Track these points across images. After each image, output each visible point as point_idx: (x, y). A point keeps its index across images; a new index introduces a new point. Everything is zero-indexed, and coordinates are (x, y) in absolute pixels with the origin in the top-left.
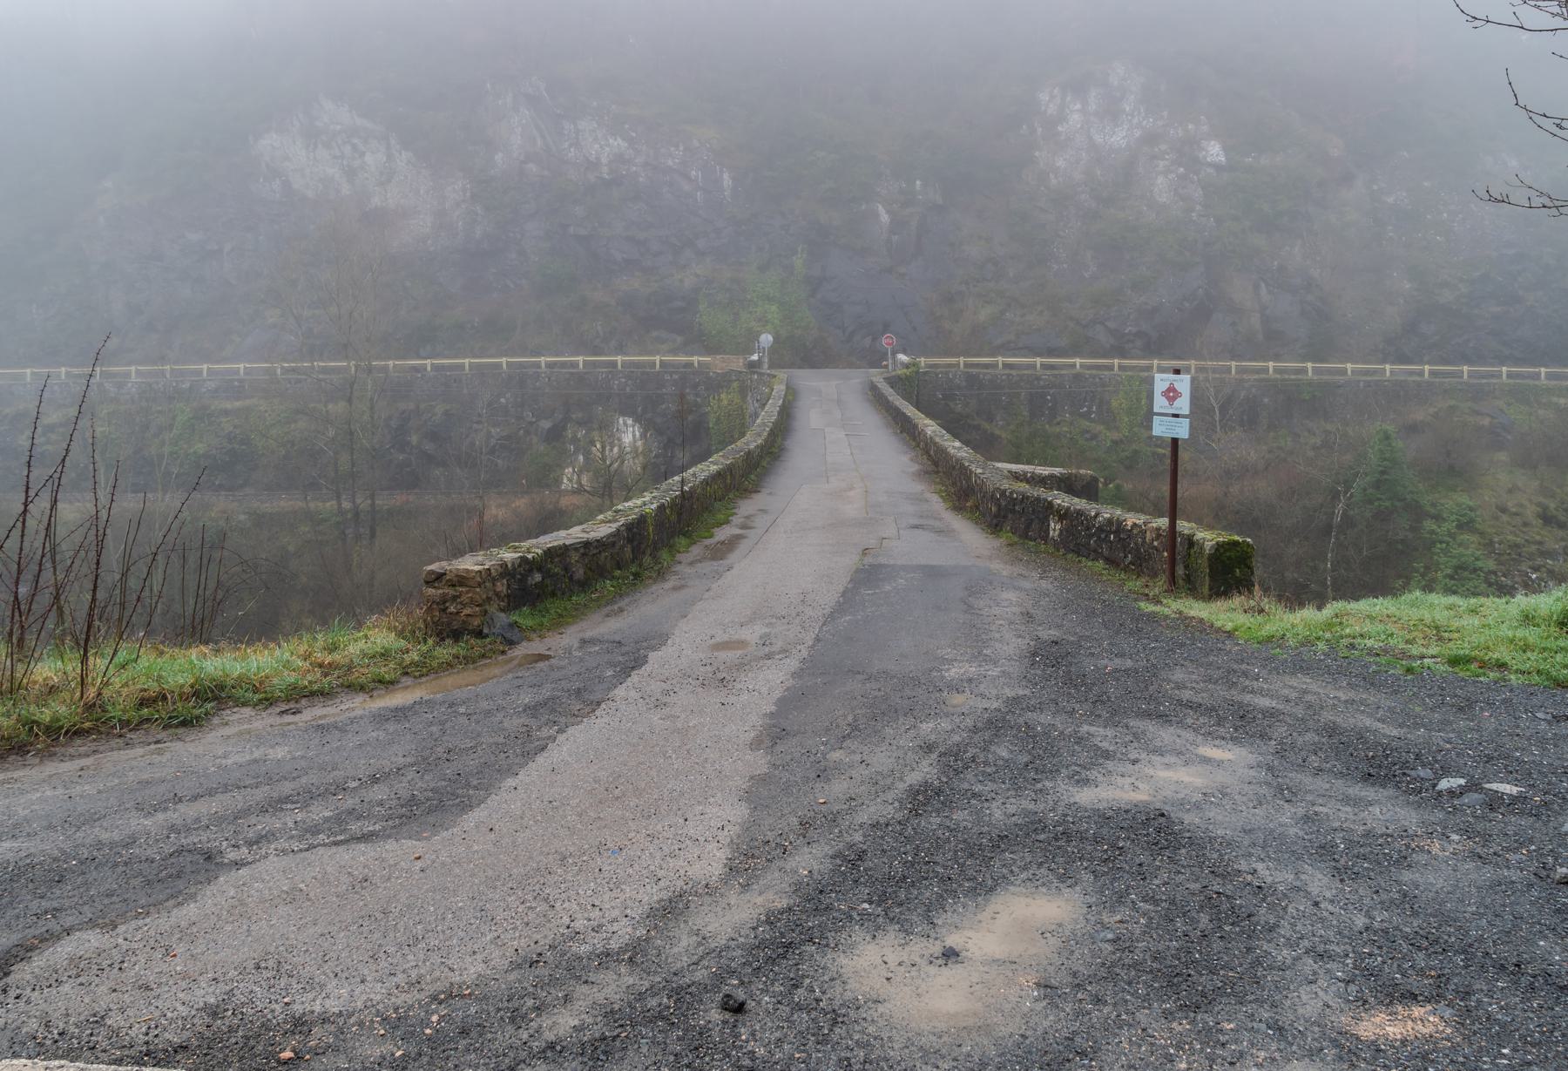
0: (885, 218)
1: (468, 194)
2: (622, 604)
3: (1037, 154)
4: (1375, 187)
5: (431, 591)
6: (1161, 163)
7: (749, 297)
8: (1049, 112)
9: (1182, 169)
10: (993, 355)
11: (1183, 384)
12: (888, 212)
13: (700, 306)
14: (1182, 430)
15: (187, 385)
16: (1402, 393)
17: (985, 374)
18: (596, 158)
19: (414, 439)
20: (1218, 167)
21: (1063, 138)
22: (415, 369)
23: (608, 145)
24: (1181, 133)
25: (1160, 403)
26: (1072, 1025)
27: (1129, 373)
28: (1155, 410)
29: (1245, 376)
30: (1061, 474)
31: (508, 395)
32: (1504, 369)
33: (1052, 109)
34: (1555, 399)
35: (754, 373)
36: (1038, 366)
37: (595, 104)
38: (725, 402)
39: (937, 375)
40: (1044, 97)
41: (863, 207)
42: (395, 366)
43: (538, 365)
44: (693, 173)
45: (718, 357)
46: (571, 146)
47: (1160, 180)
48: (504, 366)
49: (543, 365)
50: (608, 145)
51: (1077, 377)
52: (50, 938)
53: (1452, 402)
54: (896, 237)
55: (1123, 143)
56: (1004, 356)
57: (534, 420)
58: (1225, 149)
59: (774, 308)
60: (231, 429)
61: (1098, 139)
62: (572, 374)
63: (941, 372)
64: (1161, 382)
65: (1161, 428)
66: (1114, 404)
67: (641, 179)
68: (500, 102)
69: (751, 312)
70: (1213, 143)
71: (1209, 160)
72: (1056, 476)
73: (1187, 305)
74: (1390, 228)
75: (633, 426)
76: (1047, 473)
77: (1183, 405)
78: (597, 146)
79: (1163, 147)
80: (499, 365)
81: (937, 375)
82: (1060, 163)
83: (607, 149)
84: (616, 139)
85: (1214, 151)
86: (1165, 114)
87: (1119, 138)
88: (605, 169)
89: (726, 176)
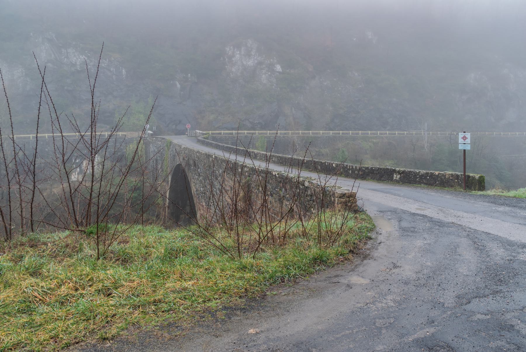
0: (179, 86)
1: (24, 74)
3: (226, 67)
4: (321, 80)
5: (342, 200)
6: (264, 71)
7: (133, 112)
8: (229, 54)
9: (270, 73)
10: (232, 130)
11: (468, 135)
12: (180, 84)
13: (116, 115)
14: (468, 148)
16: (335, 139)
17: (218, 136)
18: (75, 63)
20: (279, 72)
21: (234, 62)
23: (80, 58)
24: (269, 62)
25: (461, 141)
27: (261, 135)
29: (294, 135)
32: (360, 132)
33: (230, 53)
34: (373, 140)
35: (154, 137)
36: (234, 133)
37: (74, 43)
38: (131, 148)
40: (228, 49)
41: (172, 82)
42: (370, 133)
44: (112, 69)
45: (129, 132)
46: (65, 58)
47: (263, 76)
50: (80, 58)
51: (246, 137)
53: (348, 142)
54: (182, 92)
55: (252, 64)
56: (223, 130)
58: (282, 67)
59: (142, 116)
61: (245, 63)
62: (74, 139)
64: (461, 135)
65: (461, 147)
66: (257, 145)
67: (92, 71)
68: (37, 41)
69: (134, 117)
70: (278, 65)
73: (272, 114)
74: (326, 92)
75: (98, 157)
77: (468, 141)
78: (75, 58)
79: (264, 66)
82: (233, 70)
83: (79, 59)
84: (83, 56)
86: (264, 56)
87: (250, 63)
88: (78, 66)
89: (124, 71)
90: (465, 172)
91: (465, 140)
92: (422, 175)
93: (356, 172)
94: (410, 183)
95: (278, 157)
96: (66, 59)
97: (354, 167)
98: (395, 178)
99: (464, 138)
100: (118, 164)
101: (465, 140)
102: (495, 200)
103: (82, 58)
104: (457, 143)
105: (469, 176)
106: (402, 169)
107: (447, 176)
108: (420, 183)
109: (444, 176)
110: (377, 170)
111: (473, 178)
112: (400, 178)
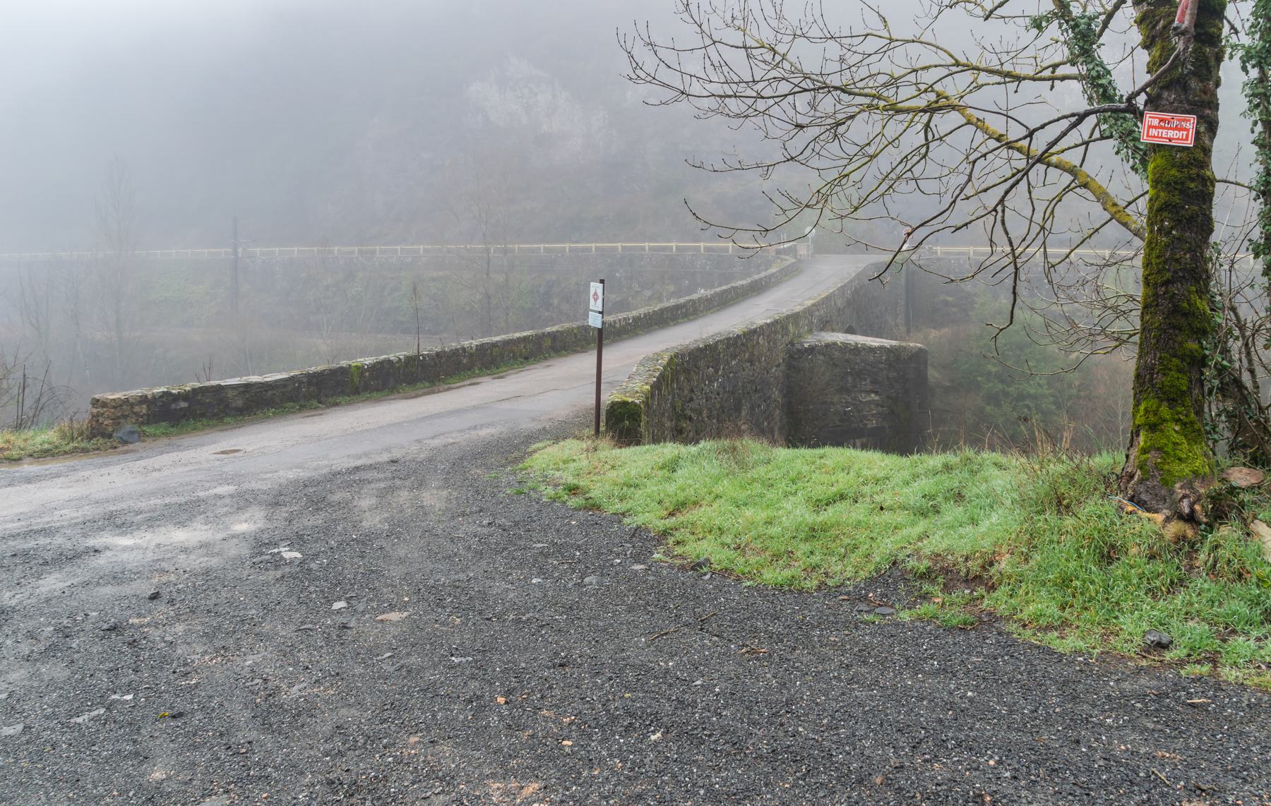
2: (339, 399)
15: (410, 260)
19: (555, 302)
22: (584, 250)
28: (591, 308)
30: (891, 346)
31: (621, 271)
39: (950, 261)
43: (643, 249)
48: (620, 250)
49: (647, 248)
52: (187, 472)
57: (640, 289)
60: (436, 291)
63: (954, 259)
72: (885, 348)
76: (877, 344)
80: (616, 248)
81: (950, 261)
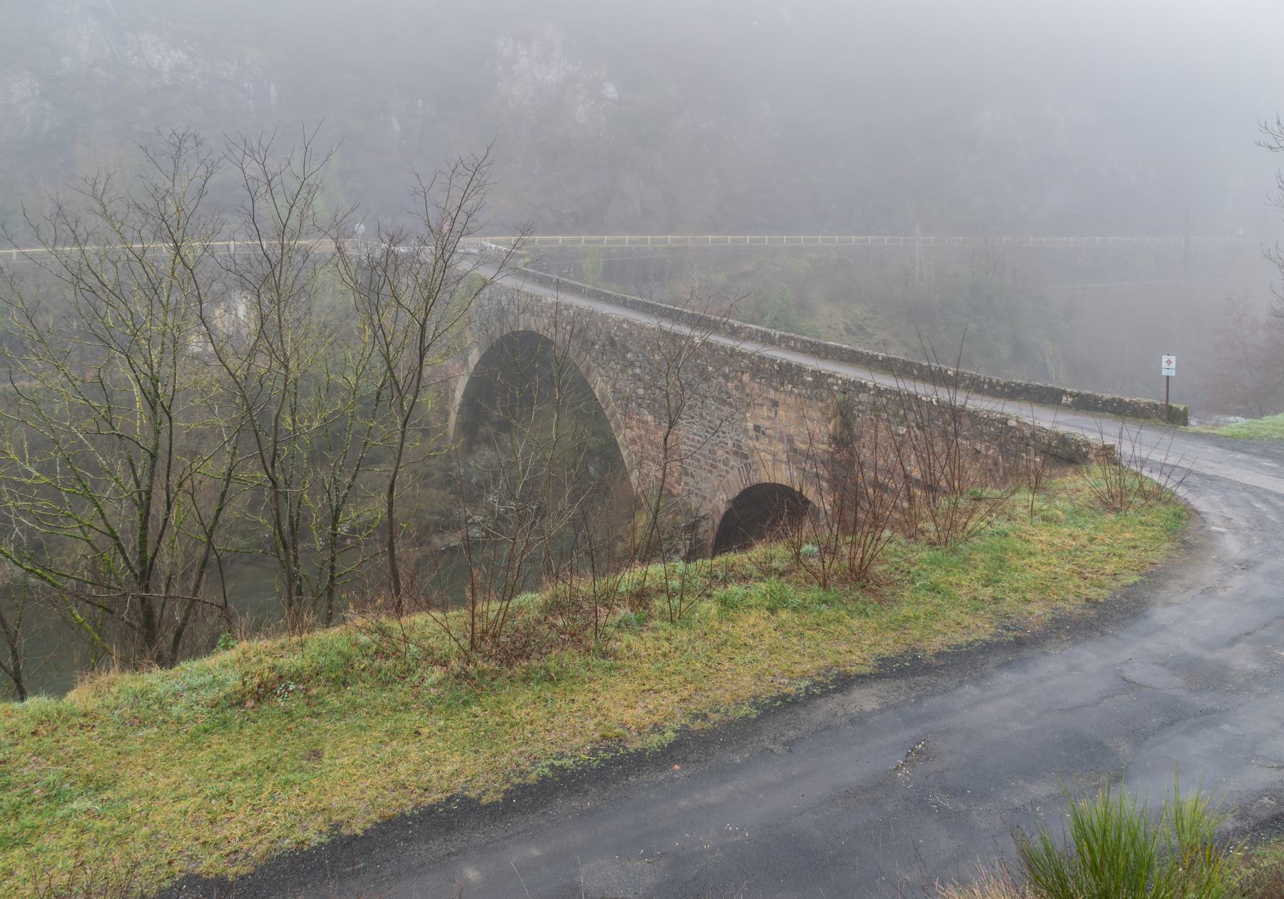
0: (397, 127)
9: (593, 102)
11: (1173, 359)
14: (1172, 373)
25: (1164, 365)
26: (73, 487)
64: (1165, 358)
65: (1165, 373)
71: (608, 95)
77: (1173, 365)
83: (169, 59)
85: (611, 90)
89: (272, 88)
90: (1167, 401)
91: (1169, 364)
92: (1107, 401)
93: (998, 388)
94: (1088, 410)
95: (803, 341)
96: (136, 58)
97: (994, 381)
98: (1063, 402)
99: (1169, 362)
100: (807, 432)
101: (1169, 364)
102: (1198, 436)
103: (177, 56)
104: (1160, 368)
105: (1171, 407)
106: (1076, 391)
107: (1141, 405)
108: (1103, 410)
109: (1137, 403)
110: (1036, 389)
111: (1177, 409)
112: (1072, 402)
